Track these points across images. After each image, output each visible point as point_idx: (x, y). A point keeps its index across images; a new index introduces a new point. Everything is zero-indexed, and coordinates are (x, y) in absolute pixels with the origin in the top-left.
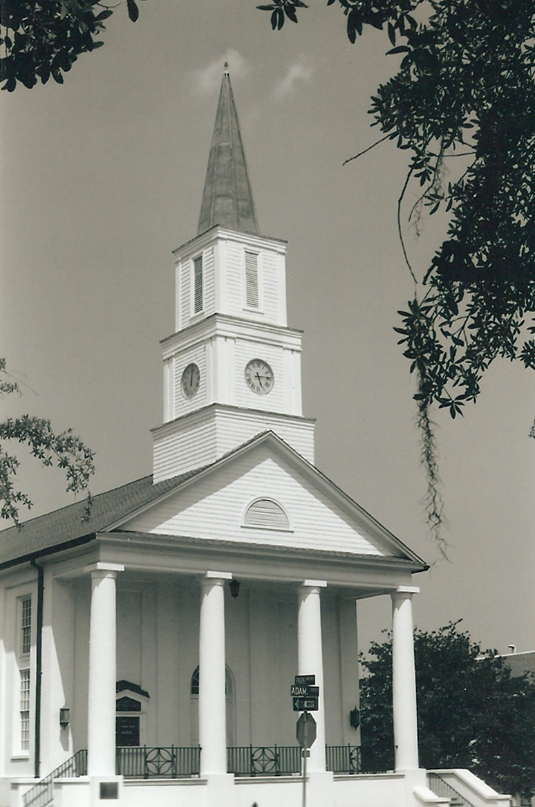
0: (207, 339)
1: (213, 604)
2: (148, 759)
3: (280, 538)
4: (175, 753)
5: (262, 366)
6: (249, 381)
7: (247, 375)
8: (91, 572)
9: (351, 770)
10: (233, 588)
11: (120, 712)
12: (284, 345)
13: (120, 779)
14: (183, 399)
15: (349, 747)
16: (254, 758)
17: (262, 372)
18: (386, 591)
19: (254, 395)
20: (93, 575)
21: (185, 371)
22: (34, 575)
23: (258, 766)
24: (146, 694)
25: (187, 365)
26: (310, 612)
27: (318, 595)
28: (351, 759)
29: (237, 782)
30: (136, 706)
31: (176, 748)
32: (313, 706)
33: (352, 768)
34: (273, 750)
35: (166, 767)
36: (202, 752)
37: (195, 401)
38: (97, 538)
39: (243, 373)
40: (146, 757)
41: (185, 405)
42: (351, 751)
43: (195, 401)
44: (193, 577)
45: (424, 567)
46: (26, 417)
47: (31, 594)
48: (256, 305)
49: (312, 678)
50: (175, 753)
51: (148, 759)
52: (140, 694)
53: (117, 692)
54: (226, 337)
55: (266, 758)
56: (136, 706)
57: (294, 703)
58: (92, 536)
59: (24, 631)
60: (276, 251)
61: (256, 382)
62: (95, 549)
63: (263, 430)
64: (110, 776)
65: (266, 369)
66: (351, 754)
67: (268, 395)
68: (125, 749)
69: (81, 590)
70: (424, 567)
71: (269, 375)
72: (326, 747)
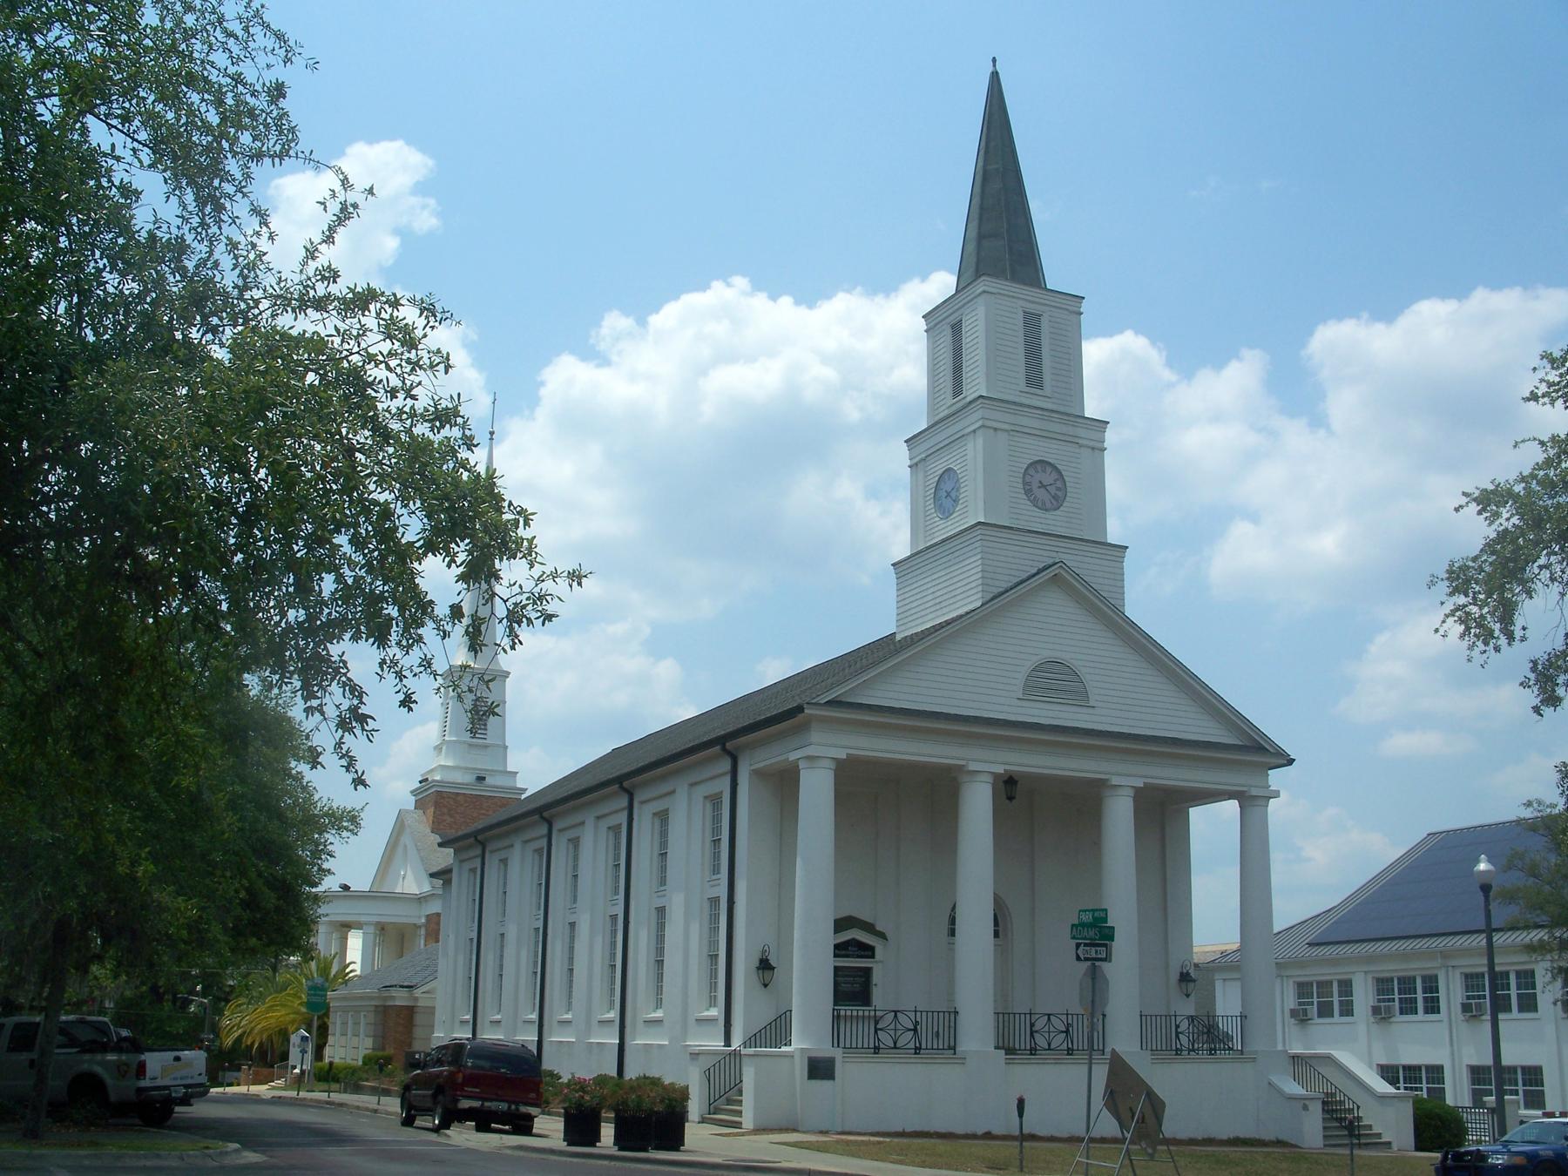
0: (970, 433)
1: (978, 805)
2: (878, 1027)
3: (1050, 714)
4: (1070, 1022)
5: (1039, 469)
6: (1028, 492)
7: (1025, 483)
8: (798, 759)
9: (1177, 1050)
10: (1008, 786)
11: (837, 959)
12: (1080, 441)
13: (838, 1054)
14: (937, 519)
15: (1030, 1014)
16: (1179, 1030)
17: (1048, 478)
18: (1230, 795)
19: (1037, 512)
20: (802, 765)
21: (939, 479)
22: (726, 765)
23: (1041, 1041)
24: (882, 936)
25: (940, 472)
26: (1120, 816)
27: (833, 772)
28: (1177, 1034)
29: (1008, 1061)
30: (867, 951)
31: (1072, 1015)
32: (1105, 956)
33: (1179, 1046)
34: (912, 1015)
35: (906, 1039)
36: (961, 1018)
37: (953, 521)
38: (806, 711)
39: (1020, 480)
40: (876, 1023)
41: (940, 528)
42: (1178, 1023)
43: (953, 521)
44: (949, 769)
45: (1288, 760)
46: (525, 516)
47: (722, 792)
48: (1041, 387)
49: (1102, 914)
50: (1070, 1022)
51: (878, 1027)
52: (875, 935)
53: (835, 933)
54: (996, 429)
55: (899, 1027)
56: (867, 951)
57: (1077, 949)
58: (799, 709)
59: (715, 845)
60: (1067, 310)
61: (1041, 494)
62: (804, 727)
63: (1051, 561)
64: (825, 1049)
65: (1055, 475)
66: (1177, 1027)
67: (1057, 512)
68: (846, 1010)
69: (785, 783)
70: (1288, 760)
71: (1059, 484)
72: (1141, 1016)
